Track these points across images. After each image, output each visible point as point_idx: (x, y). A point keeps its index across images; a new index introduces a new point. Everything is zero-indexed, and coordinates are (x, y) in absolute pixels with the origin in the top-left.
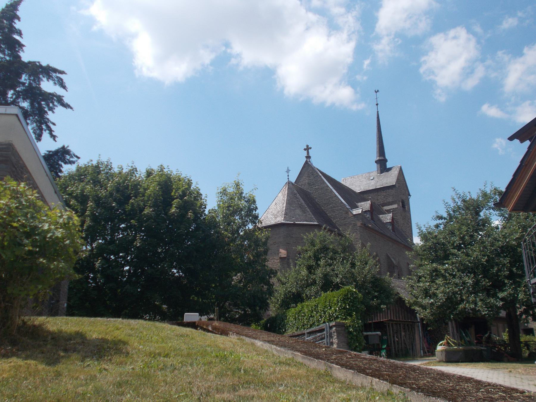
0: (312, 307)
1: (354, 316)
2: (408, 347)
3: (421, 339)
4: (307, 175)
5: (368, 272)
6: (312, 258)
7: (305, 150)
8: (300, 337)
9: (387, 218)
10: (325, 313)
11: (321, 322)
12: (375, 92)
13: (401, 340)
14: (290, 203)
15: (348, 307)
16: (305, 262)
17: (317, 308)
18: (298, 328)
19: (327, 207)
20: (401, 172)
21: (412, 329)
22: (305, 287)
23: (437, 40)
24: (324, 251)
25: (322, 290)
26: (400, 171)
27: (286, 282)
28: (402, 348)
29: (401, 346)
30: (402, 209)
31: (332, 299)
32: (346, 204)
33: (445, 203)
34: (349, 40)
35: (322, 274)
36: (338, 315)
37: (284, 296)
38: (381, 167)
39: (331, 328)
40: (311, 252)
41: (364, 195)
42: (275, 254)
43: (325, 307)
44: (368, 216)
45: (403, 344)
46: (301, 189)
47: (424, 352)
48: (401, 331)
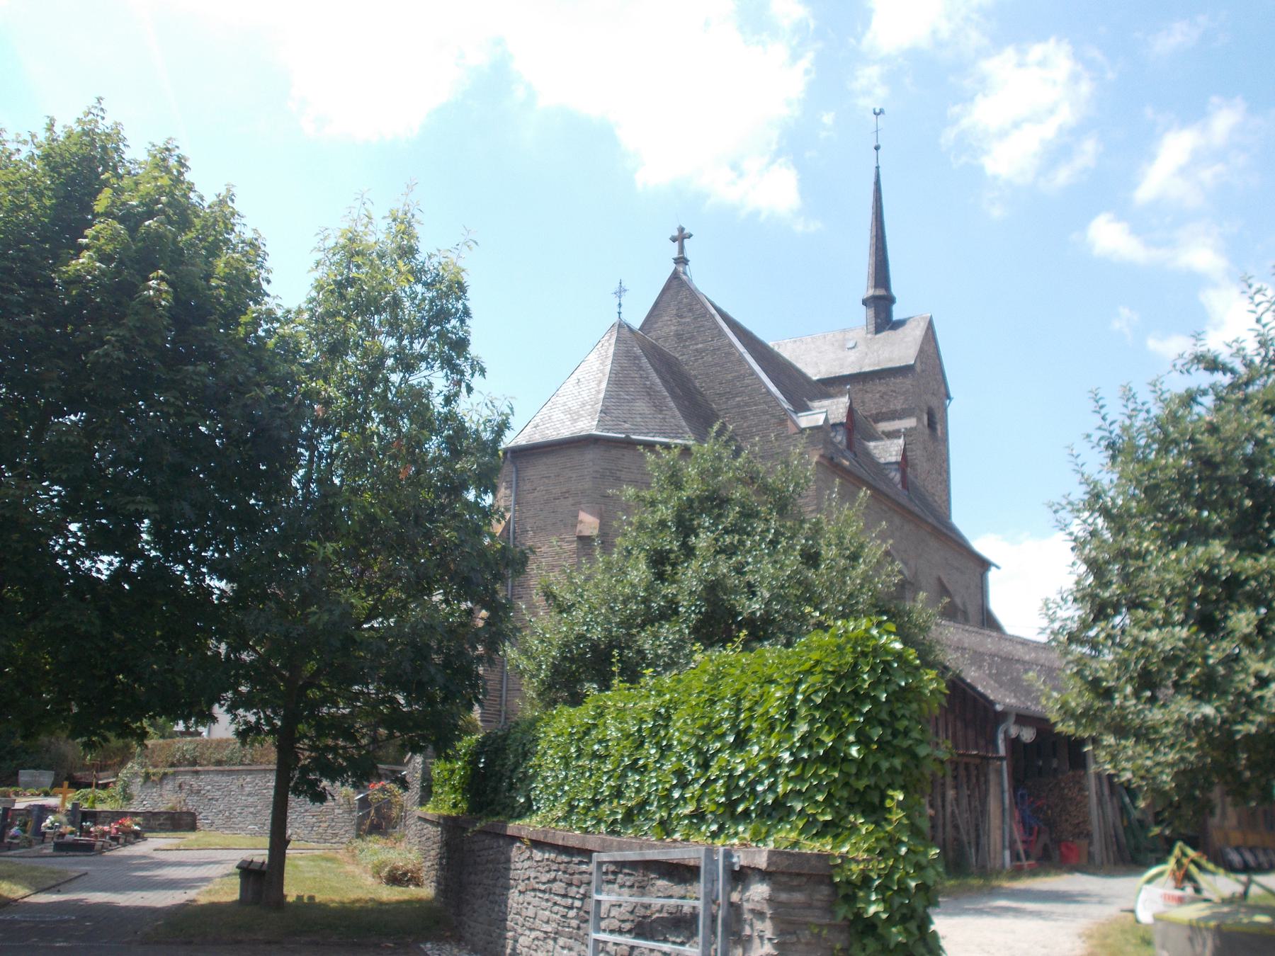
0: (642, 721)
1: (897, 815)
2: (965, 838)
3: (1007, 814)
4: (674, 312)
5: (862, 586)
6: (670, 527)
7: (674, 240)
8: (576, 860)
9: (888, 451)
10: (705, 766)
11: (680, 811)
12: (875, 113)
13: (944, 816)
14: (619, 380)
15: (854, 751)
16: (644, 539)
17: (666, 727)
18: (572, 808)
19: (726, 402)
20: (930, 332)
21: (978, 779)
22: (638, 626)
23: (1000, 66)
24: (713, 508)
25: (697, 640)
26: (928, 328)
27: (573, 605)
28: (944, 839)
29: (944, 833)
30: (927, 431)
31: (753, 690)
32: (781, 397)
33: (1253, 290)
34: (795, 57)
35: (700, 581)
36: (785, 795)
37: (561, 654)
38: (877, 315)
39: (739, 877)
40: (667, 508)
41: (829, 387)
42: (565, 525)
43: (708, 728)
44: (839, 438)
45: (949, 828)
46: (654, 347)
47: (1016, 856)
48: (943, 785)
